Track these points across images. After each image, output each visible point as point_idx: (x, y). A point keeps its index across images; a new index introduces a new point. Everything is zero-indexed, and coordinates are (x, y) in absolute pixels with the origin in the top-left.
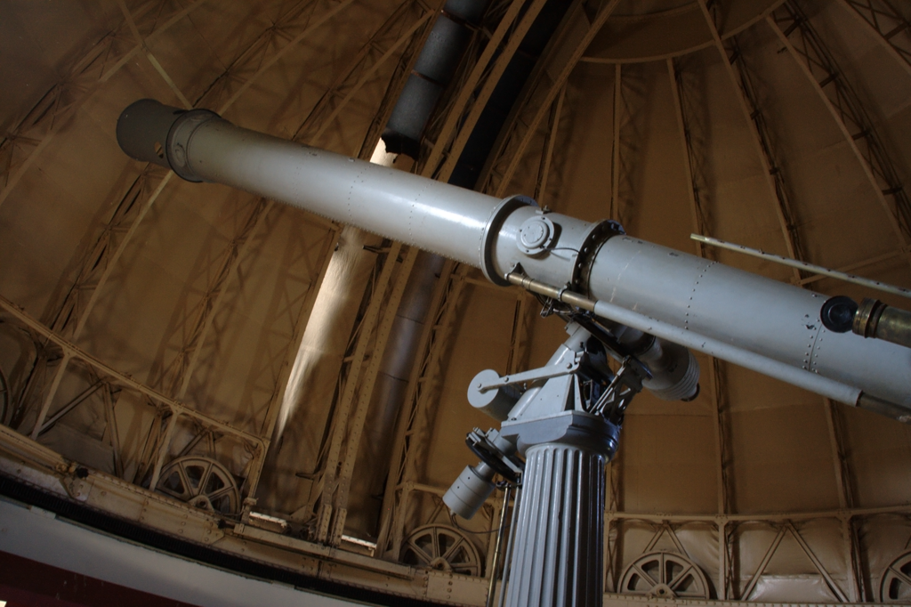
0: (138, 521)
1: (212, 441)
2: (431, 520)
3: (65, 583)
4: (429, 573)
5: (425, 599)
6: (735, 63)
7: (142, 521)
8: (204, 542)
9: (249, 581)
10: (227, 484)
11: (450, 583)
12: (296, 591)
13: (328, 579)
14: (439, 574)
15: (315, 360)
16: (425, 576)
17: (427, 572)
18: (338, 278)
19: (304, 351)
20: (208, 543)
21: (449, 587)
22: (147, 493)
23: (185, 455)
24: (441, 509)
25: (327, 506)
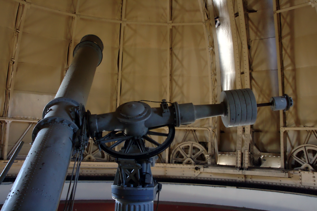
0: (165, 175)
1: (194, 132)
2: (306, 142)
3: (76, 210)
4: (301, 173)
5: (302, 187)
6: (86, 111)
7: (166, 175)
8: (193, 176)
9: (216, 188)
10: (201, 149)
11: (314, 177)
12: (237, 189)
13: (251, 182)
14: (306, 172)
15: (233, 77)
16: (300, 174)
17: (300, 172)
18: (228, 36)
19: (227, 76)
20: (195, 176)
21: (314, 179)
22: (165, 165)
23: (184, 141)
24: (311, 134)
25: (239, 151)
